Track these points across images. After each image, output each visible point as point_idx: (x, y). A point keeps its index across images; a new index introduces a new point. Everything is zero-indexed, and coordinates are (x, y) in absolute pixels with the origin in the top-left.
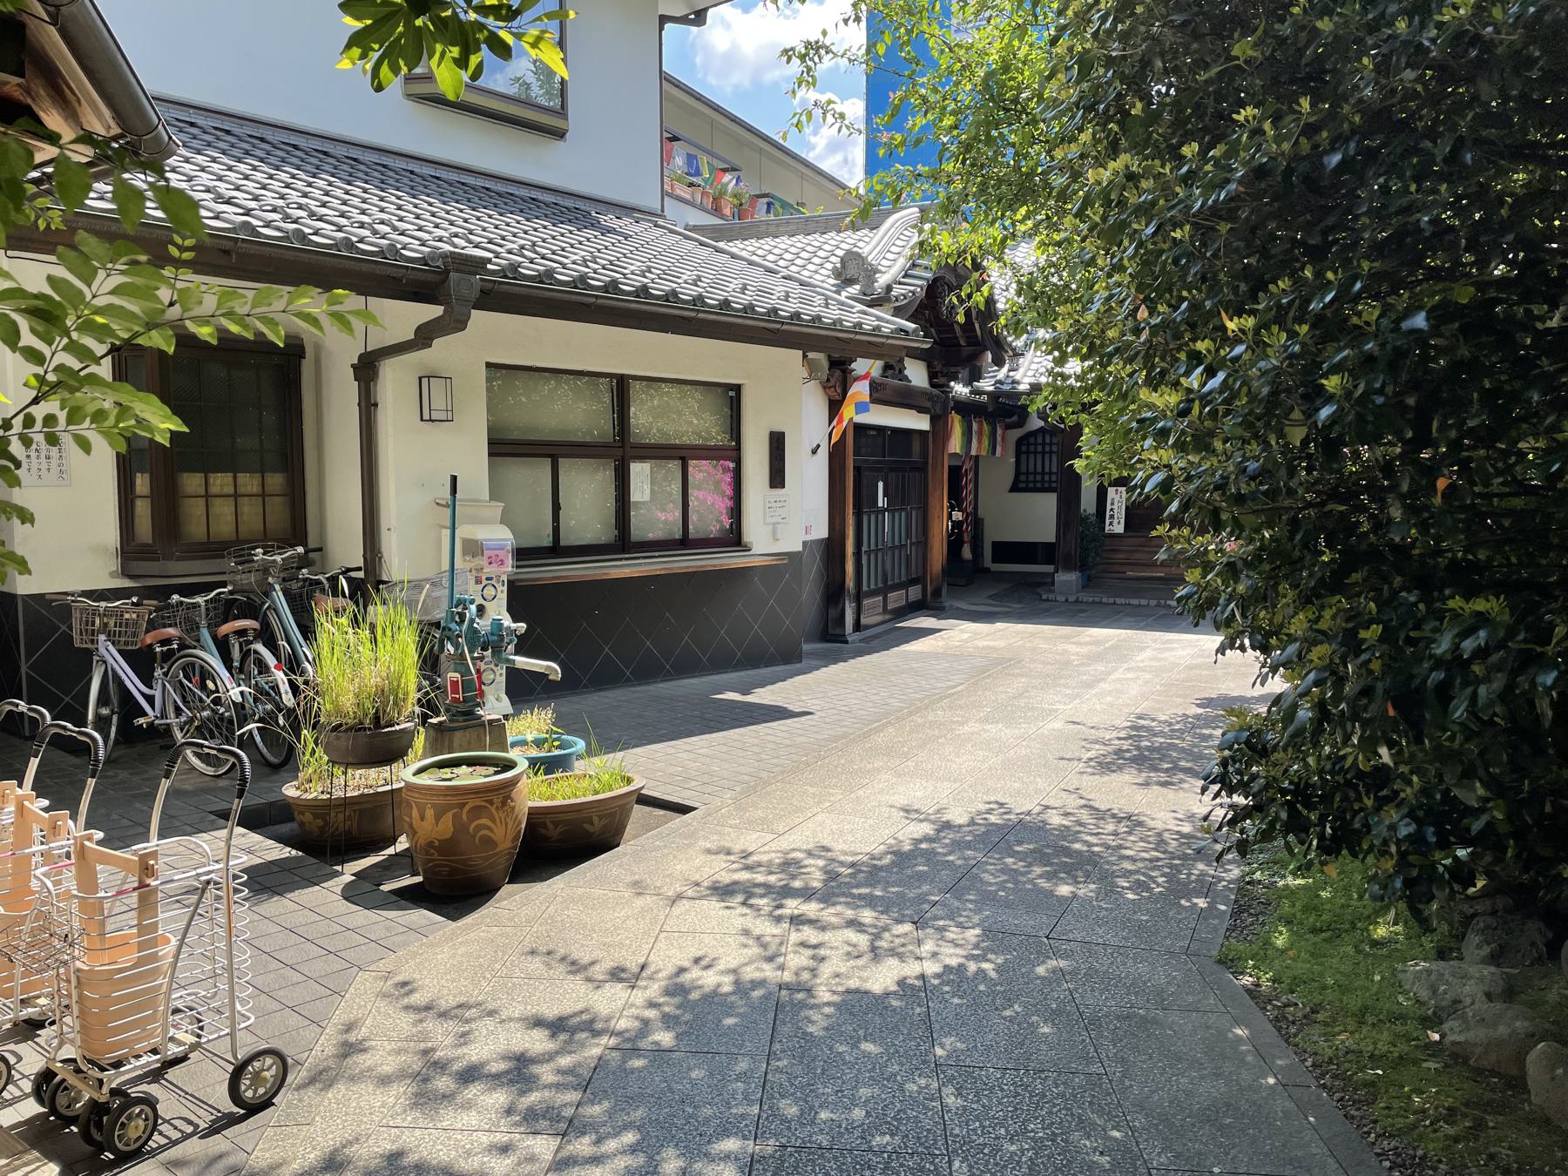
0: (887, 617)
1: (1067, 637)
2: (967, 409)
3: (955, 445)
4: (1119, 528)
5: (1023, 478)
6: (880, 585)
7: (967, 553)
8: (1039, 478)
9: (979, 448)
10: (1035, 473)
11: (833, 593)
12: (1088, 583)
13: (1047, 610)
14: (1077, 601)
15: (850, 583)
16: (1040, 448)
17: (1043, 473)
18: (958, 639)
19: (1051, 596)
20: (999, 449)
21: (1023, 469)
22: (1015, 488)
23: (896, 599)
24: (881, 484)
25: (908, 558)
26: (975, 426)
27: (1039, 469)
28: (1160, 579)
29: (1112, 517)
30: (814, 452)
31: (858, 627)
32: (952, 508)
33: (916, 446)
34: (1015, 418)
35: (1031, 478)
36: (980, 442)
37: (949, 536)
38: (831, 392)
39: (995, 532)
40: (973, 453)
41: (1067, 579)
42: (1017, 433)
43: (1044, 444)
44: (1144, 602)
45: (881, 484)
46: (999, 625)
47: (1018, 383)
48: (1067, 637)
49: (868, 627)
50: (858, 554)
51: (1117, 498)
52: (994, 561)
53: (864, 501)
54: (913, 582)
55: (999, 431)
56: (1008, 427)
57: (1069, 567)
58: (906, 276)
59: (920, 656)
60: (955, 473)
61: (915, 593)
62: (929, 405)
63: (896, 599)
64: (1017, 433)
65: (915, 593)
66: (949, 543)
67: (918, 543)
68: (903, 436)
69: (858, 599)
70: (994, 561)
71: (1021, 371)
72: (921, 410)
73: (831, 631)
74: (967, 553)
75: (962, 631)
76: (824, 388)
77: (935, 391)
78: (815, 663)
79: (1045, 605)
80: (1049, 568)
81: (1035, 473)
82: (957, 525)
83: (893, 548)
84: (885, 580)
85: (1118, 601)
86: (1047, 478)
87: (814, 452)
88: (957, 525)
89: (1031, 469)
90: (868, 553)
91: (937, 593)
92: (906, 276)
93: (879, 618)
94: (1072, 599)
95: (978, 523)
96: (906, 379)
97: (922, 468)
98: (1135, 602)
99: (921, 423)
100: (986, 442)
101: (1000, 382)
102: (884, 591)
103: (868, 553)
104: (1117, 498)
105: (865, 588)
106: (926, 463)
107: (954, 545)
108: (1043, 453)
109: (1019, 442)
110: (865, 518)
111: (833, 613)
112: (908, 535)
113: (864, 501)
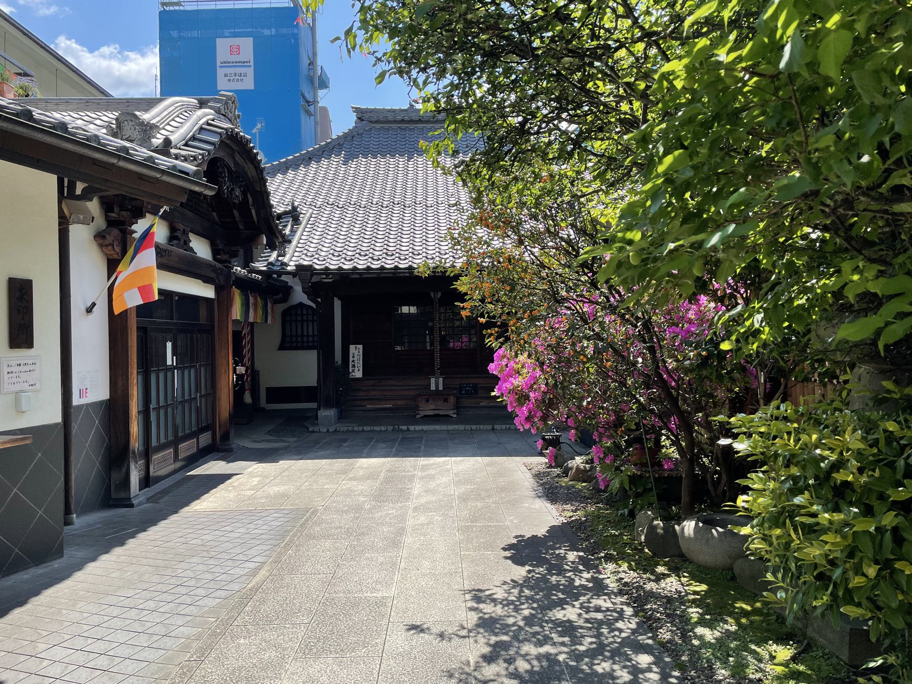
0: (179, 464)
1: (344, 472)
2: (245, 285)
3: (237, 312)
4: (358, 374)
5: (288, 339)
6: (170, 438)
7: (248, 398)
8: (299, 339)
9: (255, 316)
10: (297, 336)
11: (116, 455)
12: (341, 417)
13: (317, 442)
14: (335, 431)
15: (136, 443)
16: (299, 318)
17: (302, 336)
18: (254, 486)
19: (316, 429)
20: (269, 318)
21: (288, 333)
22: (282, 347)
23: (187, 448)
24: (169, 345)
25: (198, 410)
26: (251, 300)
27: (300, 333)
28: (389, 409)
29: (354, 366)
30: (89, 310)
31: (146, 481)
32: (236, 363)
33: (203, 312)
34: (281, 295)
35: (294, 339)
36: (255, 311)
37: (235, 386)
38: (109, 250)
39: (271, 378)
40: (251, 320)
41: (327, 414)
42: (281, 307)
43: (302, 315)
44: (383, 428)
45: (169, 345)
46: (283, 464)
47: (287, 265)
48: (344, 472)
49: (159, 479)
50: (145, 413)
51: (356, 353)
52: (267, 402)
53: (150, 361)
54: (202, 430)
55: (269, 305)
56: (275, 302)
57: (328, 405)
58: (186, 145)
59: (218, 518)
60: (237, 336)
61: (205, 439)
62: (213, 275)
63: (187, 448)
64: (281, 307)
65: (205, 439)
66: (235, 392)
67: (207, 395)
68: (195, 300)
69: (147, 454)
70: (267, 402)
71: (288, 256)
72: (206, 280)
73: (114, 495)
74: (248, 398)
75: (252, 475)
76: (101, 246)
77: (219, 265)
78: (81, 554)
79: (314, 437)
80: (314, 405)
81: (297, 336)
82: (240, 377)
83: (183, 403)
84: (176, 436)
85: (366, 428)
86: (305, 339)
87: (89, 310)
88: (240, 377)
89: (311, 333)
90: (158, 409)
91: (226, 437)
92: (186, 145)
93: (172, 467)
94: (331, 430)
95: (254, 373)
96: (192, 250)
97: (208, 330)
98: (377, 428)
99: (208, 292)
100: (260, 312)
101: (271, 264)
102: (175, 443)
103: (158, 409)
104: (356, 353)
105: (154, 443)
106: (213, 326)
107: (238, 393)
108: (302, 321)
109: (285, 314)
110: (153, 377)
111: (116, 476)
112: (198, 389)
113: (150, 361)
